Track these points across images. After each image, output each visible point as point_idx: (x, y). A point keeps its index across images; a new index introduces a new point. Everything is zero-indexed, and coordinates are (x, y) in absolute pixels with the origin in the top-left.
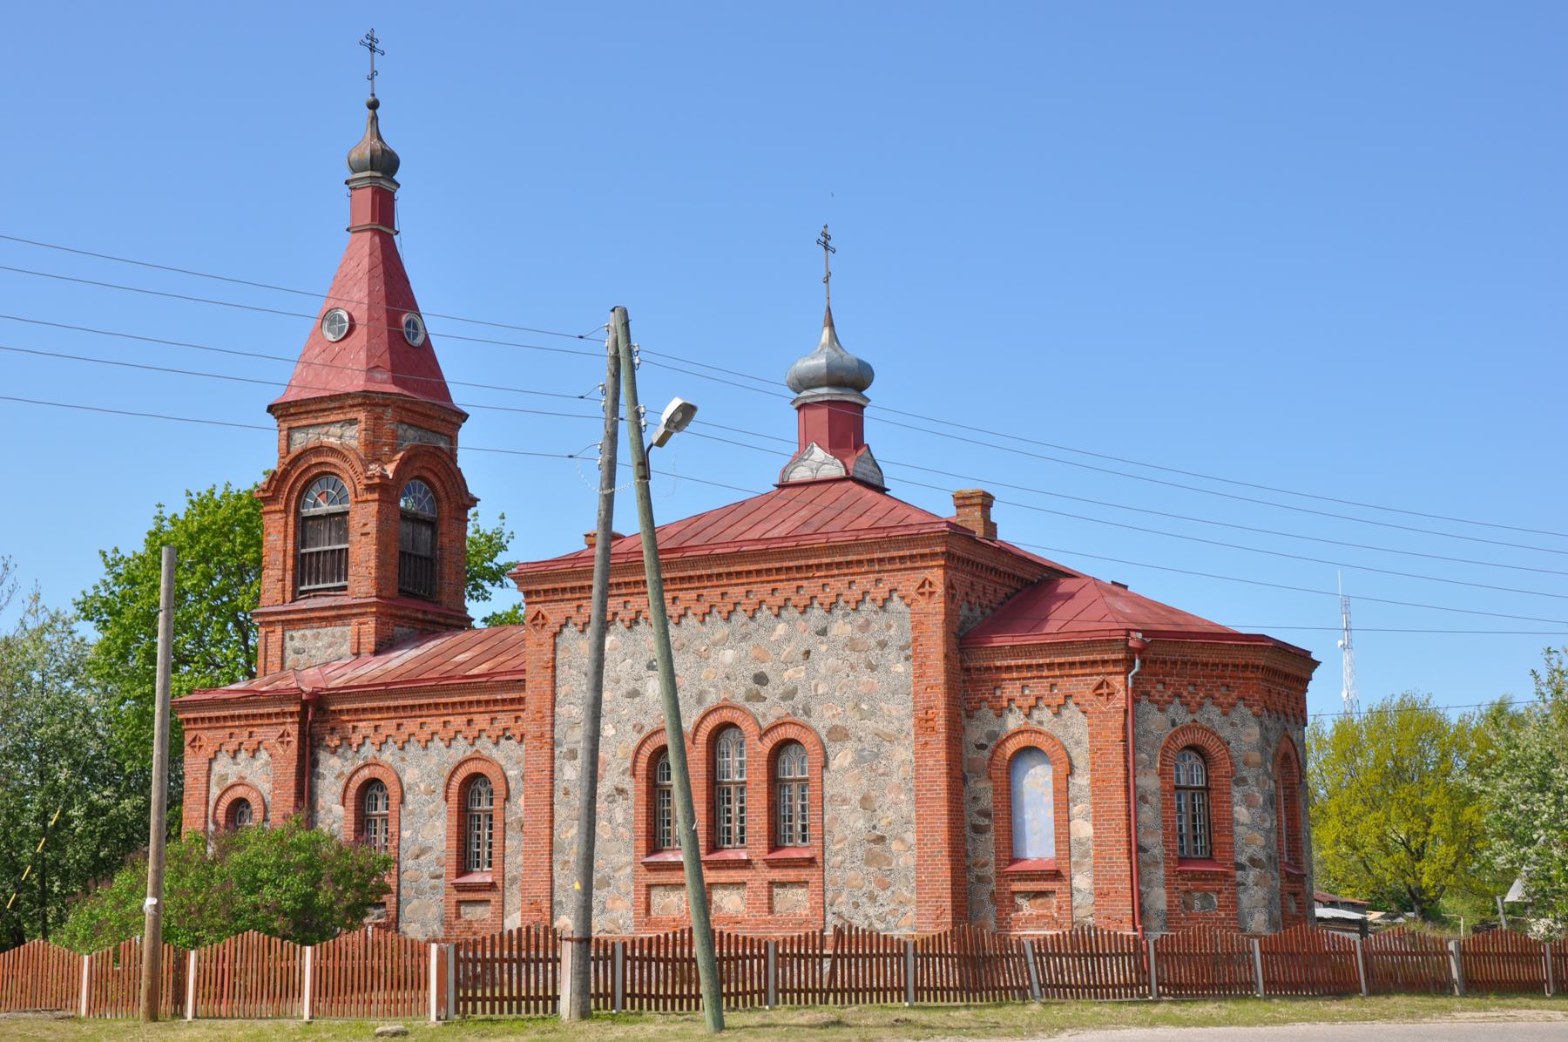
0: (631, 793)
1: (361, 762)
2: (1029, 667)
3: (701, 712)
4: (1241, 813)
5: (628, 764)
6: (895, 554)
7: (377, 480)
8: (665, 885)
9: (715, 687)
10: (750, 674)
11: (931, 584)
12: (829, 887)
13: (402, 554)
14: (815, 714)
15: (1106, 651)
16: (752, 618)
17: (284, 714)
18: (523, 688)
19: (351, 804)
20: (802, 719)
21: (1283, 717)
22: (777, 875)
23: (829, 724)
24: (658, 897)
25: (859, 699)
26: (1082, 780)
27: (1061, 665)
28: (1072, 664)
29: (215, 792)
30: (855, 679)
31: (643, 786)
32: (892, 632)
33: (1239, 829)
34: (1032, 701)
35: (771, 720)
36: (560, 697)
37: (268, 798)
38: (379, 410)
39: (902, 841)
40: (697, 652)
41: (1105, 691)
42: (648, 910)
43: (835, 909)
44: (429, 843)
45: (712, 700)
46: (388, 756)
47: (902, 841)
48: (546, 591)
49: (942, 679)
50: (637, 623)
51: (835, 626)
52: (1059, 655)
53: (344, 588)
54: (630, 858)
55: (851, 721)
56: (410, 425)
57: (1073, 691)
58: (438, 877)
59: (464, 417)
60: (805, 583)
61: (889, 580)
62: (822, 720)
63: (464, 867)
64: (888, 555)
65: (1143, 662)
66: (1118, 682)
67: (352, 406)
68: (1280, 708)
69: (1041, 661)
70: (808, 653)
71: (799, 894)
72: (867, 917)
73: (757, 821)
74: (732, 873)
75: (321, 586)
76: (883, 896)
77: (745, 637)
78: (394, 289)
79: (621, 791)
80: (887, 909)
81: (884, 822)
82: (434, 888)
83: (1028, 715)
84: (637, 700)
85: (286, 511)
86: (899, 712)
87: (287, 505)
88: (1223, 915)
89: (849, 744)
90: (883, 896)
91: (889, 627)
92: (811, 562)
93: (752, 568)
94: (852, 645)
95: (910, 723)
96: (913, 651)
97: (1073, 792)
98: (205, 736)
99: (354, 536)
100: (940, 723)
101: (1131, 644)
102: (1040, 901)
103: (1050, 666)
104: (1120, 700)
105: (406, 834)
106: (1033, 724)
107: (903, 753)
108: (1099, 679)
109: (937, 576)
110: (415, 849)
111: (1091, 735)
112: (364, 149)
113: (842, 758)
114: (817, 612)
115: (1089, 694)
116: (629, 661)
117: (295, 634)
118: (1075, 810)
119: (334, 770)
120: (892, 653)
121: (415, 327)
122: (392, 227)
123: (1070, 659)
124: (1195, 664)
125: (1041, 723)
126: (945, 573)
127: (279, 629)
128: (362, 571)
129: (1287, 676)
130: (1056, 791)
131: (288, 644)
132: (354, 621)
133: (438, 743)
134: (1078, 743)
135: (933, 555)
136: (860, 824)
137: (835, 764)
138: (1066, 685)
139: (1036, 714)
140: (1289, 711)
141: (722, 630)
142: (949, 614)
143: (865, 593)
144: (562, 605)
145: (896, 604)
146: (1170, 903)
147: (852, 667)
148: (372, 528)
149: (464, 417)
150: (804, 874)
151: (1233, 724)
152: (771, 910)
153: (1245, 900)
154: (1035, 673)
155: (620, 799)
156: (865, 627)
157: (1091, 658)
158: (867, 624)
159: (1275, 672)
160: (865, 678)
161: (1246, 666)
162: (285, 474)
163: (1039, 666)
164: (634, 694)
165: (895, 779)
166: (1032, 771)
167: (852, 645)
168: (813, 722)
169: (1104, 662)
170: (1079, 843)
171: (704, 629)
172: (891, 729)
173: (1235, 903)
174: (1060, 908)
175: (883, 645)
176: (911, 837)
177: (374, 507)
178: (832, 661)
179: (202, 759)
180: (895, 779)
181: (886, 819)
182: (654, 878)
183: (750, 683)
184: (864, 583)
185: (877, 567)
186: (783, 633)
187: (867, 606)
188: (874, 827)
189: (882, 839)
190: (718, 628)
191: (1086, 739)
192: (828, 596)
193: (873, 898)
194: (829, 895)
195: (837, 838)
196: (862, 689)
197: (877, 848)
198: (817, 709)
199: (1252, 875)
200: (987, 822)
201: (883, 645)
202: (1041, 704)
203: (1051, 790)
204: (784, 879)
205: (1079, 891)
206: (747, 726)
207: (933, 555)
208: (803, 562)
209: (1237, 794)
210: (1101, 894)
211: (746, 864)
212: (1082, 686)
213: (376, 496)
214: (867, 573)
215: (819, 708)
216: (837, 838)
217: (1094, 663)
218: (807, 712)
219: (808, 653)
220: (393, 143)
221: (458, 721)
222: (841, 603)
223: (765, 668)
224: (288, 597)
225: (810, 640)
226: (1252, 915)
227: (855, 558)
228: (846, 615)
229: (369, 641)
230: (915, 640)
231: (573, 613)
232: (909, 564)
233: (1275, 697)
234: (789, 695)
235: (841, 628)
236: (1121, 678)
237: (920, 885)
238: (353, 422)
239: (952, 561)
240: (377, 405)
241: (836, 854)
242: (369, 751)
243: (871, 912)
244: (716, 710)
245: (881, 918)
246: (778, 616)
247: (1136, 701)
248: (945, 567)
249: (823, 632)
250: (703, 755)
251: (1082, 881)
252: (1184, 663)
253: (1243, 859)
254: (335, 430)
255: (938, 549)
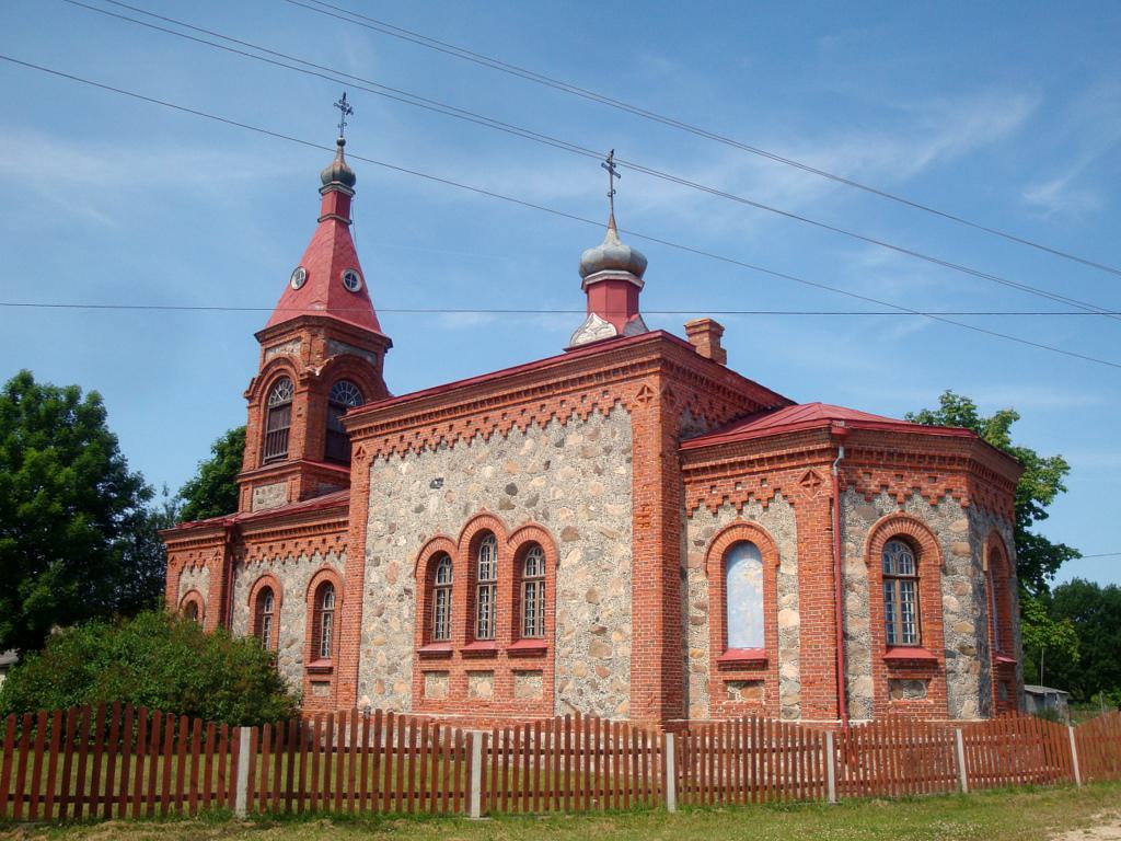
0: (414, 592)
1: (260, 574)
2: (742, 464)
3: (466, 520)
4: (951, 601)
5: (412, 569)
6: (618, 365)
7: (306, 377)
8: (436, 672)
9: (478, 499)
10: (503, 486)
11: (649, 389)
12: (558, 675)
13: (328, 431)
14: (552, 518)
15: (811, 442)
16: (506, 437)
17: (214, 540)
18: (347, 514)
19: (253, 605)
20: (541, 523)
21: (992, 516)
22: (517, 664)
23: (563, 525)
24: (473, 682)
25: (588, 502)
26: (789, 570)
27: (770, 459)
28: (781, 458)
29: (181, 595)
30: (582, 484)
31: (422, 587)
32: (616, 438)
33: (948, 617)
34: (744, 497)
35: (518, 524)
36: (371, 515)
37: (206, 600)
38: (315, 330)
39: (621, 631)
40: (466, 471)
41: (812, 481)
42: (422, 692)
43: (563, 696)
44: (296, 636)
45: (474, 511)
46: (276, 570)
47: (621, 631)
48: (365, 430)
49: (657, 477)
50: (425, 450)
51: (570, 437)
52: (768, 450)
53: (286, 456)
54: (411, 648)
55: (582, 522)
56: (341, 342)
57: (781, 484)
58: (300, 662)
59: (388, 343)
60: (547, 402)
61: (615, 390)
62: (555, 527)
63: (315, 656)
64: (612, 367)
65: (848, 452)
66: (824, 471)
67: (299, 328)
68: (988, 504)
69: (752, 457)
70: (548, 463)
71: (535, 682)
72: (589, 703)
73: (504, 617)
74: (483, 661)
75: (273, 456)
76: (604, 684)
77: (501, 454)
78: (345, 255)
79: (408, 591)
80: (605, 696)
81: (605, 614)
82: (297, 670)
83: (740, 511)
84: (422, 514)
85: (259, 406)
86: (620, 511)
87: (260, 401)
88: (932, 702)
89: (578, 543)
90: (604, 684)
91: (614, 434)
92: (550, 382)
93: (506, 393)
94: (585, 454)
95: (629, 520)
96: (635, 457)
97: (782, 581)
98: (178, 556)
99: (294, 418)
100: (656, 518)
101: (834, 431)
102: (750, 689)
103: (761, 461)
104: (828, 487)
105: (283, 628)
106: (744, 518)
107: (624, 549)
108: (806, 470)
109: (654, 382)
110: (288, 641)
111: (799, 526)
112: (327, 162)
113: (572, 557)
114: (555, 425)
115: (796, 485)
116: (418, 482)
117: (260, 490)
118: (783, 600)
119: (246, 577)
120: (616, 457)
121: (354, 279)
122: (348, 217)
123: (778, 453)
124: (901, 455)
125: (752, 517)
126: (662, 379)
127: (250, 487)
128: (297, 442)
129: (995, 476)
130: (766, 582)
131: (255, 496)
132: (289, 478)
133: (304, 559)
134: (786, 535)
135: (651, 363)
136: (587, 616)
137: (564, 563)
138: (776, 478)
139: (747, 510)
140: (997, 509)
141: (485, 450)
142: (664, 418)
143: (595, 404)
144: (375, 440)
145: (620, 412)
146: (877, 690)
147: (584, 473)
148: (303, 412)
149: (388, 343)
150: (325, 678)
151: (941, 515)
152: (512, 695)
153: (954, 685)
154: (748, 470)
155: (406, 597)
156: (595, 435)
157: (797, 450)
158: (597, 432)
159: (983, 469)
160: (593, 482)
161: (952, 459)
162: (260, 379)
163: (750, 462)
164: (419, 509)
165: (616, 573)
166: (740, 563)
167: (585, 454)
168: (549, 526)
169: (810, 453)
170: (787, 632)
171: (471, 450)
172: (614, 527)
173: (946, 690)
174: (768, 696)
175: (608, 450)
176: (628, 628)
177: (306, 395)
178: (569, 469)
179: (176, 574)
180: (616, 573)
181: (608, 610)
182: (427, 665)
183: (503, 493)
184: (594, 395)
185: (604, 381)
186: (529, 447)
187: (597, 417)
188: (597, 620)
189: (603, 630)
190: (481, 449)
191: (794, 530)
192: (563, 411)
193: (595, 686)
194: (558, 683)
195: (567, 629)
196: (590, 492)
197: (599, 639)
198: (553, 512)
199: (963, 662)
200: (703, 614)
201: (608, 450)
202: (752, 499)
203: (761, 582)
204: (523, 668)
205: (786, 679)
206: (498, 532)
207: (651, 363)
208: (544, 383)
209: (946, 582)
210: (806, 682)
211: (493, 654)
212: (790, 479)
213: (307, 388)
214: (596, 386)
215: (555, 512)
216: (567, 629)
217: (801, 454)
218: (546, 516)
219: (548, 463)
220: (353, 165)
221: (317, 540)
222: (575, 416)
223: (515, 480)
224: (257, 465)
225: (550, 452)
226: (962, 702)
227: (585, 373)
228: (579, 426)
229: (297, 490)
230: (635, 442)
231: (382, 446)
232: (631, 374)
233: (983, 493)
234: (532, 502)
235: (574, 440)
236: (826, 468)
237: (633, 678)
238: (298, 339)
239: (668, 369)
240: (313, 326)
241: (566, 645)
242: (265, 565)
243: (593, 700)
244: (476, 518)
245: (601, 705)
246: (525, 433)
247: (841, 491)
248: (660, 373)
249: (560, 444)
250: (466, 558)
251: (789, 670)
252: (891, 454)
253: (953, 647)
254: (290, 347)
255: (654, 357)
